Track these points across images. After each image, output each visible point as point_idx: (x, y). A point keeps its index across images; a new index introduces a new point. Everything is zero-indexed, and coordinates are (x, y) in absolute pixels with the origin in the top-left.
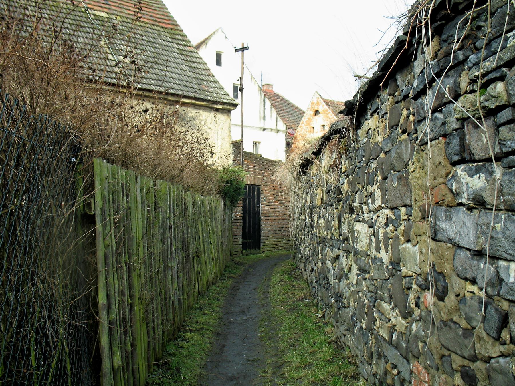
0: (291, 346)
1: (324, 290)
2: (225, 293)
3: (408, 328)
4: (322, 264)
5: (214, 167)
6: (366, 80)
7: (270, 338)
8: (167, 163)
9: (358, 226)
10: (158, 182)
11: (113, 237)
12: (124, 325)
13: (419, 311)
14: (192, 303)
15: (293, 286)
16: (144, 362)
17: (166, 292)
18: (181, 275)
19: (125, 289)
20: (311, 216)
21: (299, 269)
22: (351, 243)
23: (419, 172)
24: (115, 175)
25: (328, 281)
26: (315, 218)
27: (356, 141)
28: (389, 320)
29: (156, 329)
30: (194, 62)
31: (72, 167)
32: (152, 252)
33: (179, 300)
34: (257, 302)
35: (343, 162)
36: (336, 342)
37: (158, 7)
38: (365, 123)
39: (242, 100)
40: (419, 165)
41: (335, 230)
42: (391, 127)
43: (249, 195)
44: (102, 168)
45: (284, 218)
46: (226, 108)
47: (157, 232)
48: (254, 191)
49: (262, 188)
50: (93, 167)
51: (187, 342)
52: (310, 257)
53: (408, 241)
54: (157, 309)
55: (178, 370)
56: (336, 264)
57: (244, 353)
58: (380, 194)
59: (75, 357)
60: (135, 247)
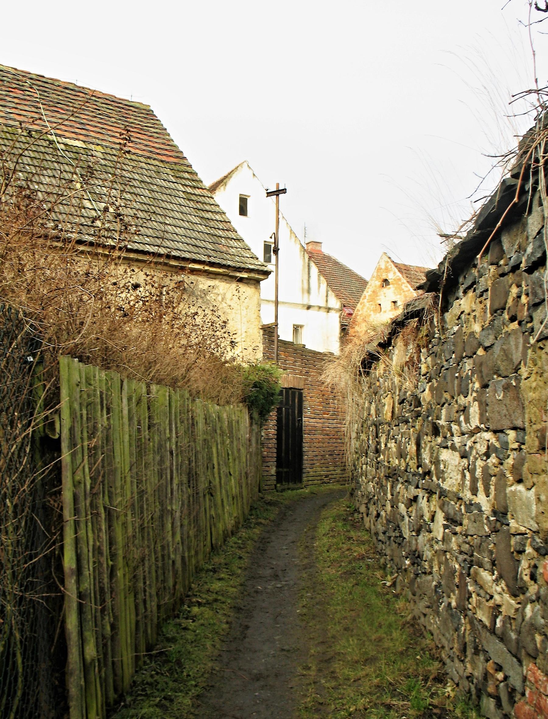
0: (345, 629)
1: (394, 546)
2: (250, 548)
3: (520, 611)
4: (392, 507)
5: (235, 363)
6: (457, 241)
7: (314, 617)
8: (167, 360)
9: (445, 455)
10: (154, 388)
11: (87, 470)
12: (101, 598)
13: (536, 587)
14: (202, 562)
15: (350, 538)
16: (129, 652)
17: (163, 547)
18: (186, 522)
19: (103, 545)
20: (377, 437)
21: (359, 512)
22: (434, 478)
23: (535, 380)
24: (90, 380)
25: (401, 532)
26: (383, 440)
27: (444, 329)
28: (492, 597)
29: (148, 602)
30: (207, 211)
31: (28, 369)
32: (143, 491)
33: (183, 558)
34: (297, 561)
35: (423, 359)
36: (413, 625)
37: (156, 133)
38: (456, 303)
39: (277, 265)
40: (535, 369)
41: (411, 458)
42: (494, 311)
43: (287, 403)
44: (71, 370)
45: (337, 436)
46: (254, 277)
47: (151, 460)
48: (294, 396)
49: (305, 393)
50: (59, 368)
51: (194, 621)
52: (374, 496)
53: (520, 481)
54: (149, 573)
55: (179, 663)
56: (413, 509)
57: (277, 638)
58: (477, 409)
59: (30, 649)
60: (119, 484)
